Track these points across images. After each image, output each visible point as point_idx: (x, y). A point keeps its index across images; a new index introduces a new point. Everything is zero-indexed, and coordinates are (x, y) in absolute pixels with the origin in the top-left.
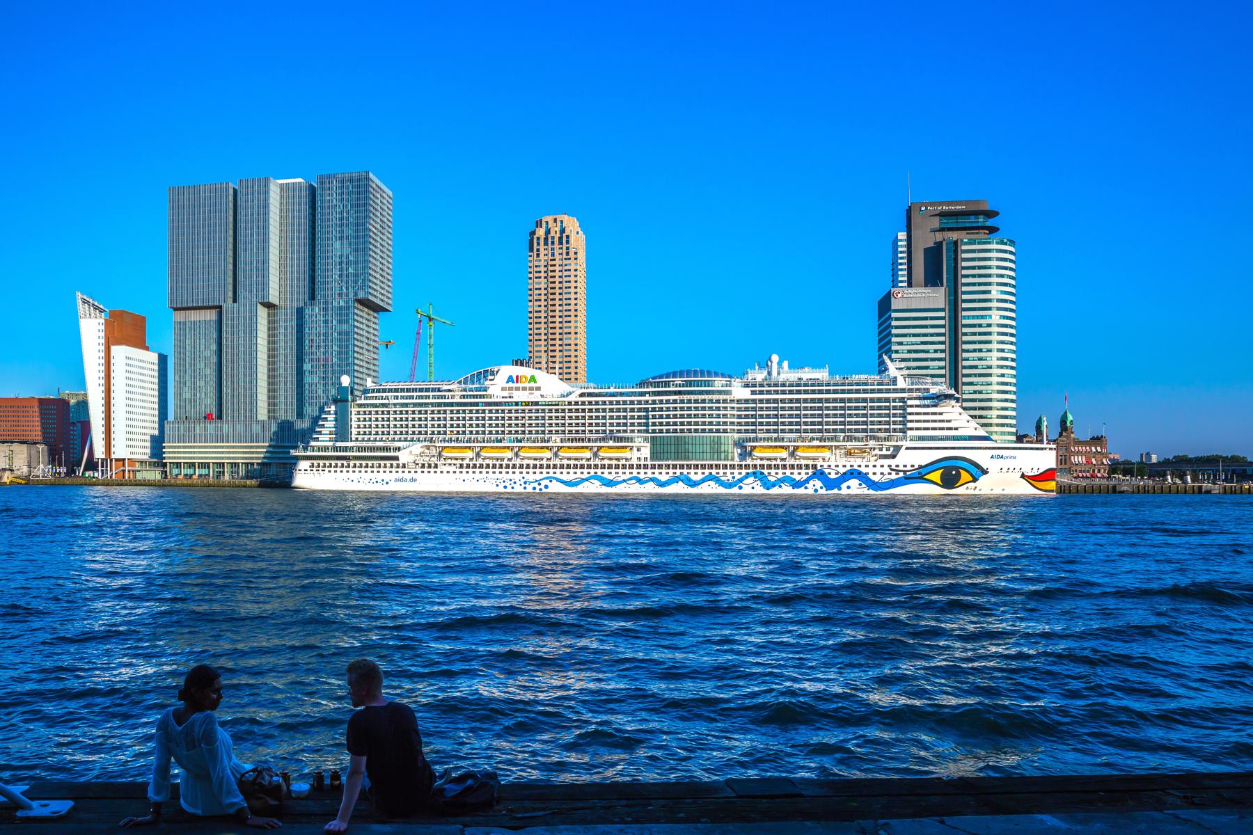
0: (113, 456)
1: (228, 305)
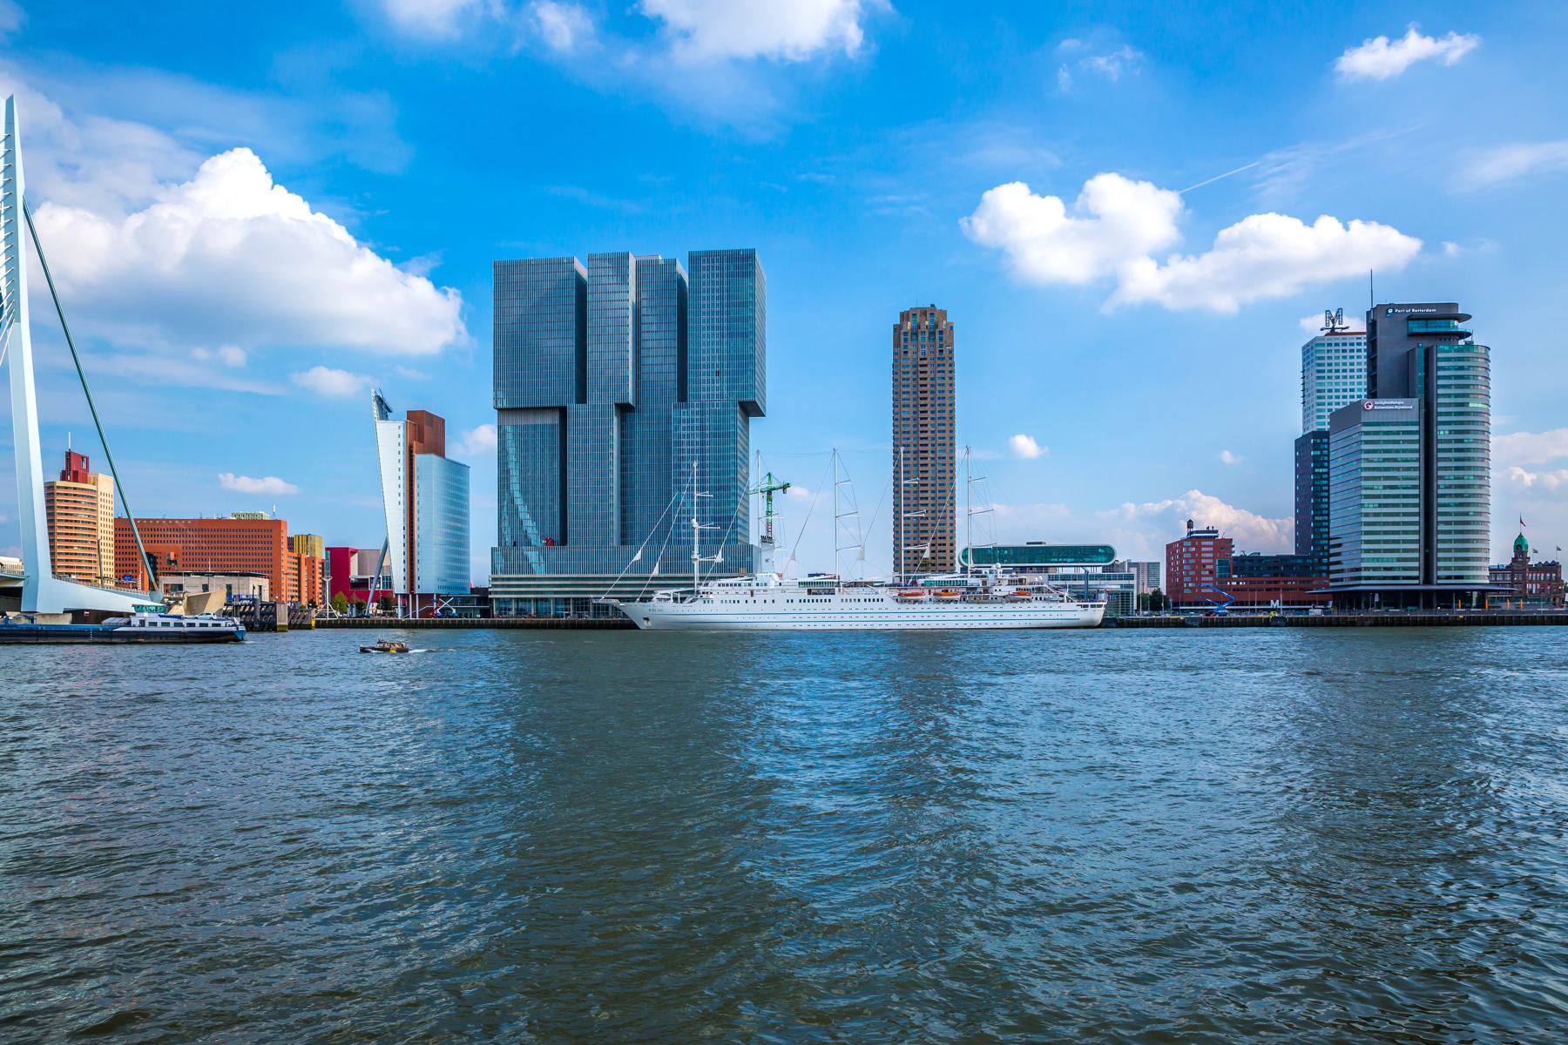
0: (417, 591)
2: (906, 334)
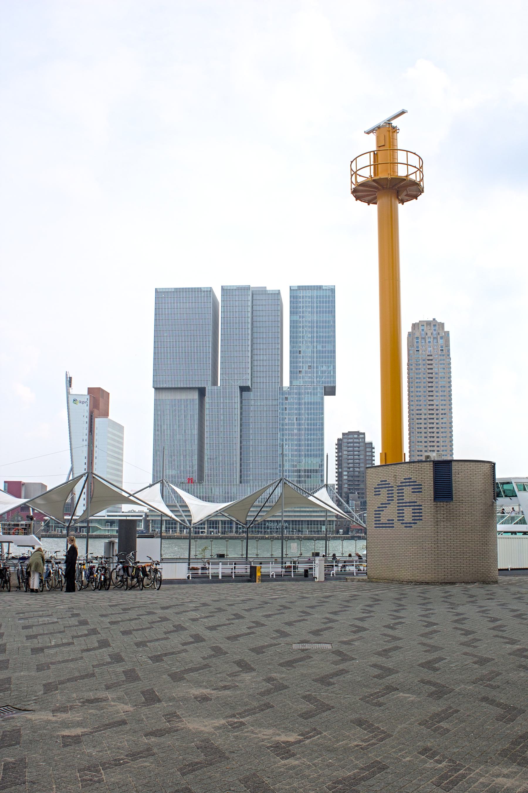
1: (209, 388)
2: (417, 338)
